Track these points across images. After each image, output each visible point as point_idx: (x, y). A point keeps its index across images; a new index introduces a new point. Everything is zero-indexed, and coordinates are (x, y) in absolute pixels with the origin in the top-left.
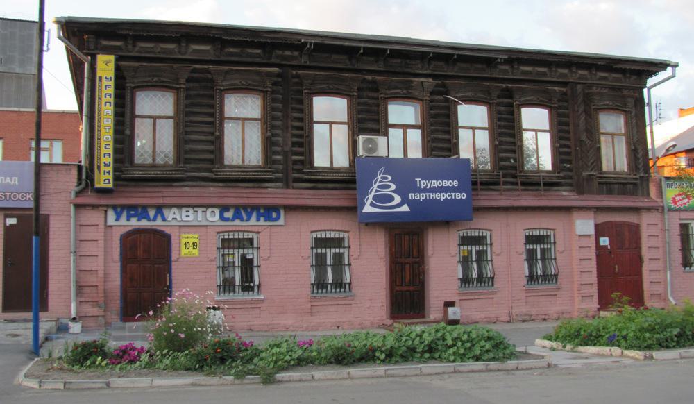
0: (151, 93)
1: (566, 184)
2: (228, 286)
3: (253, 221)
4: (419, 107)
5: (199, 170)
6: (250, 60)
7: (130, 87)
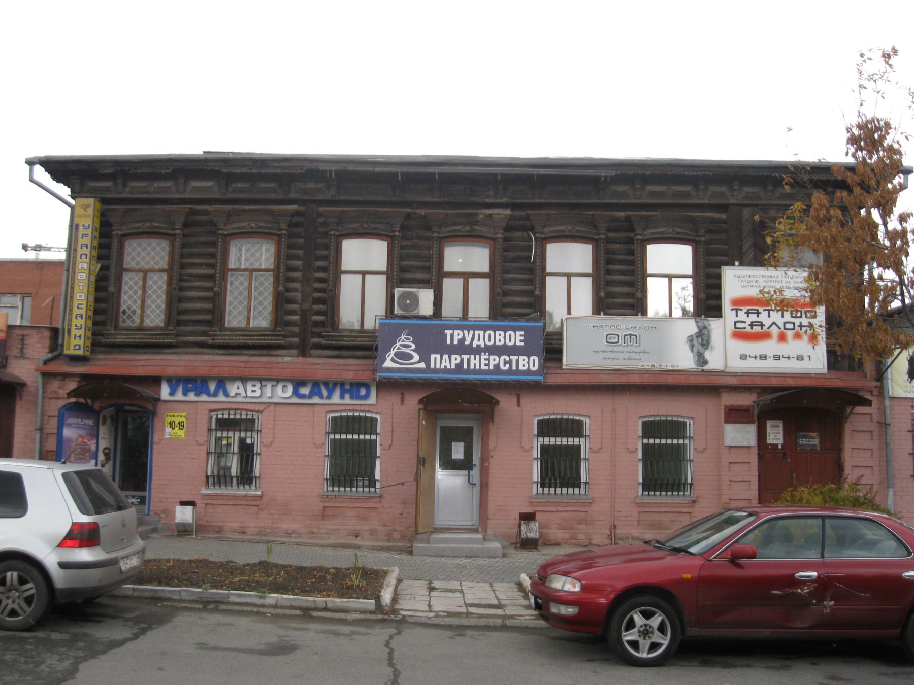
1: (289, 347)
5: (196, 334)
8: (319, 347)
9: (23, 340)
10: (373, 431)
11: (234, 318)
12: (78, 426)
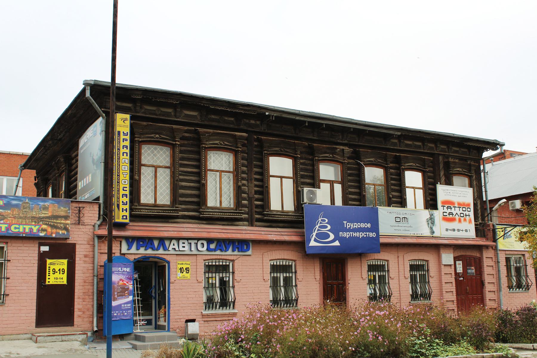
0: (152, 147)
2: (210, 302)
3: (230, 252)
4: (339, 167)
6: (226, 125)
7: (138, 141)
8: (258, 220)
9: (79, 211)
11: (212, 201)
12: (123, 273)
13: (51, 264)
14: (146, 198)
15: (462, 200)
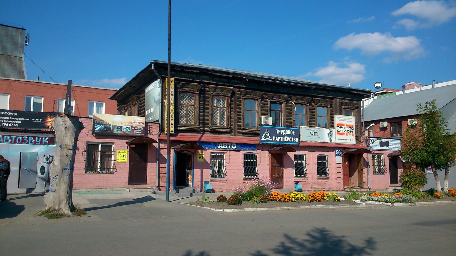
10: (254, 159)
13: (119, 152)
14: (183, 120)
15: (349, 123)
